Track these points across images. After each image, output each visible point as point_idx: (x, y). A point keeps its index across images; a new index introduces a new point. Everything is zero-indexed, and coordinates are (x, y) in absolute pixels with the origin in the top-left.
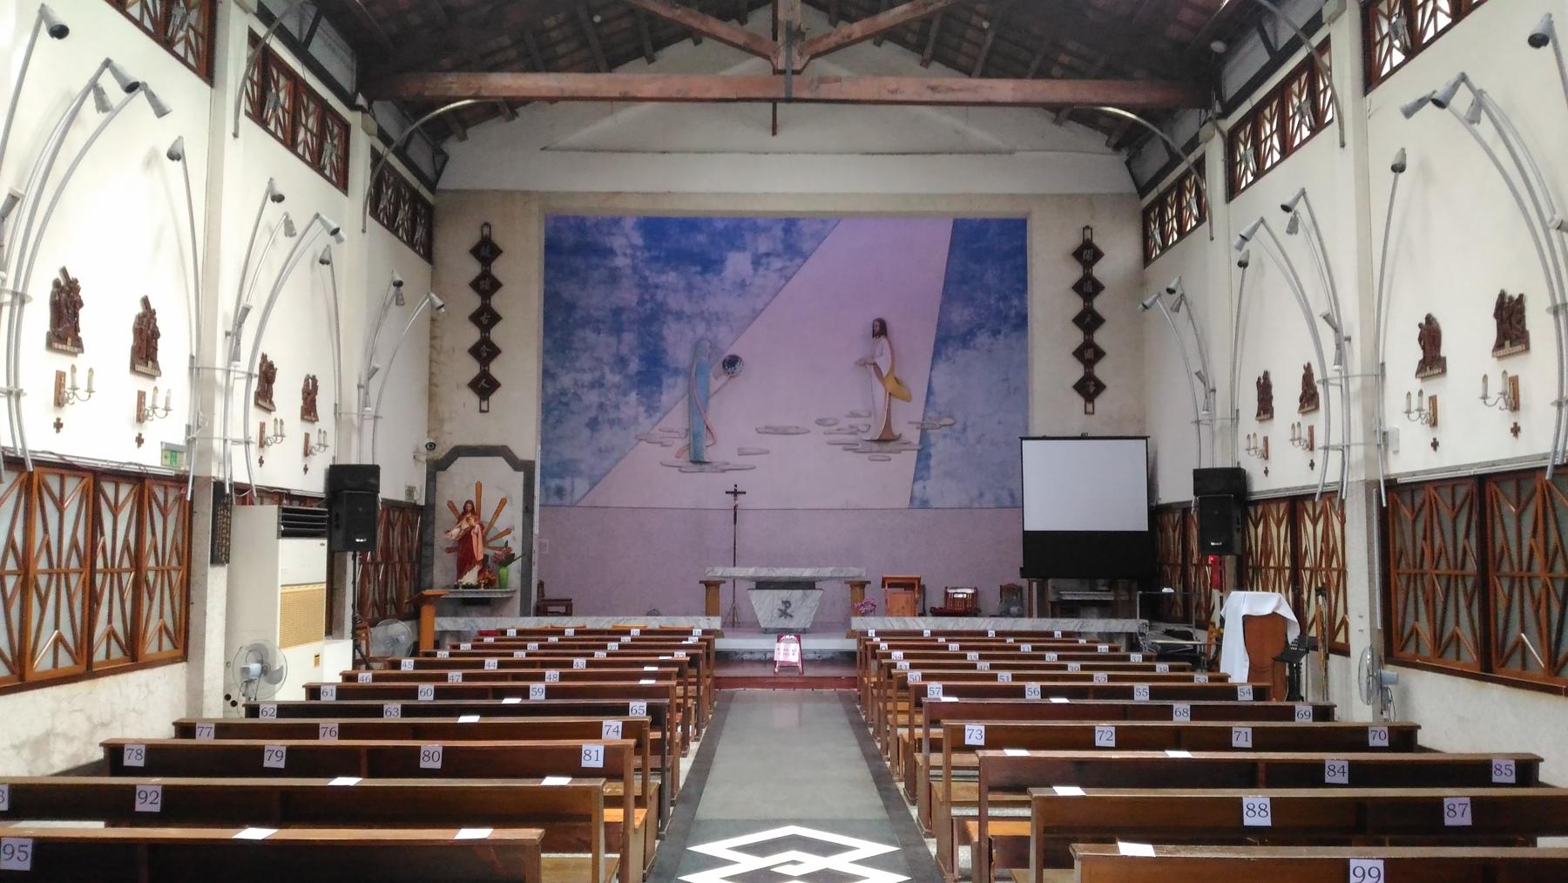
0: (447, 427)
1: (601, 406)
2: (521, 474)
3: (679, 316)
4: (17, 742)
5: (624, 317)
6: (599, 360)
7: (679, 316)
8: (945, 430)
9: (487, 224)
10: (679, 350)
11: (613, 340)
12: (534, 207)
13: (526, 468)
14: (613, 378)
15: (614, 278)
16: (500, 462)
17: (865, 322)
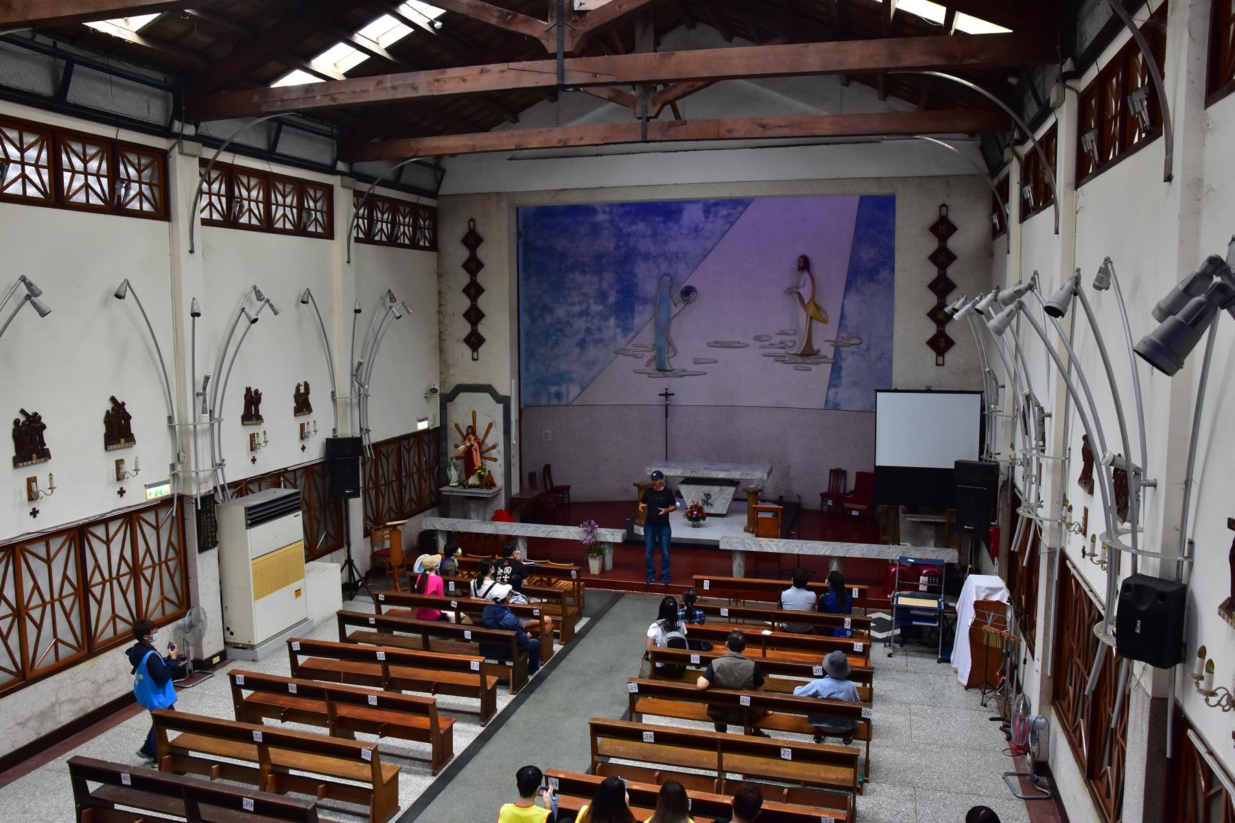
0: (452, 371)
1: (588, 330)
2: (501, 406)
3: (647, 257)
4: (22, 720)
5: (604, 261)
6: (586, 295)
7: (647, 257)
8: (853, 348)
9: (472, 220)
10: (648, 284)
11: (596, 279)
12: (504, 205)
13: (504, 401)
14: (596, 308)
15: (596, 230)
16: (487, 396)
17: (792, 260)
